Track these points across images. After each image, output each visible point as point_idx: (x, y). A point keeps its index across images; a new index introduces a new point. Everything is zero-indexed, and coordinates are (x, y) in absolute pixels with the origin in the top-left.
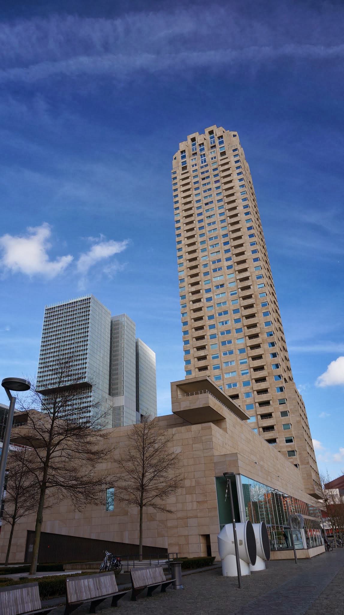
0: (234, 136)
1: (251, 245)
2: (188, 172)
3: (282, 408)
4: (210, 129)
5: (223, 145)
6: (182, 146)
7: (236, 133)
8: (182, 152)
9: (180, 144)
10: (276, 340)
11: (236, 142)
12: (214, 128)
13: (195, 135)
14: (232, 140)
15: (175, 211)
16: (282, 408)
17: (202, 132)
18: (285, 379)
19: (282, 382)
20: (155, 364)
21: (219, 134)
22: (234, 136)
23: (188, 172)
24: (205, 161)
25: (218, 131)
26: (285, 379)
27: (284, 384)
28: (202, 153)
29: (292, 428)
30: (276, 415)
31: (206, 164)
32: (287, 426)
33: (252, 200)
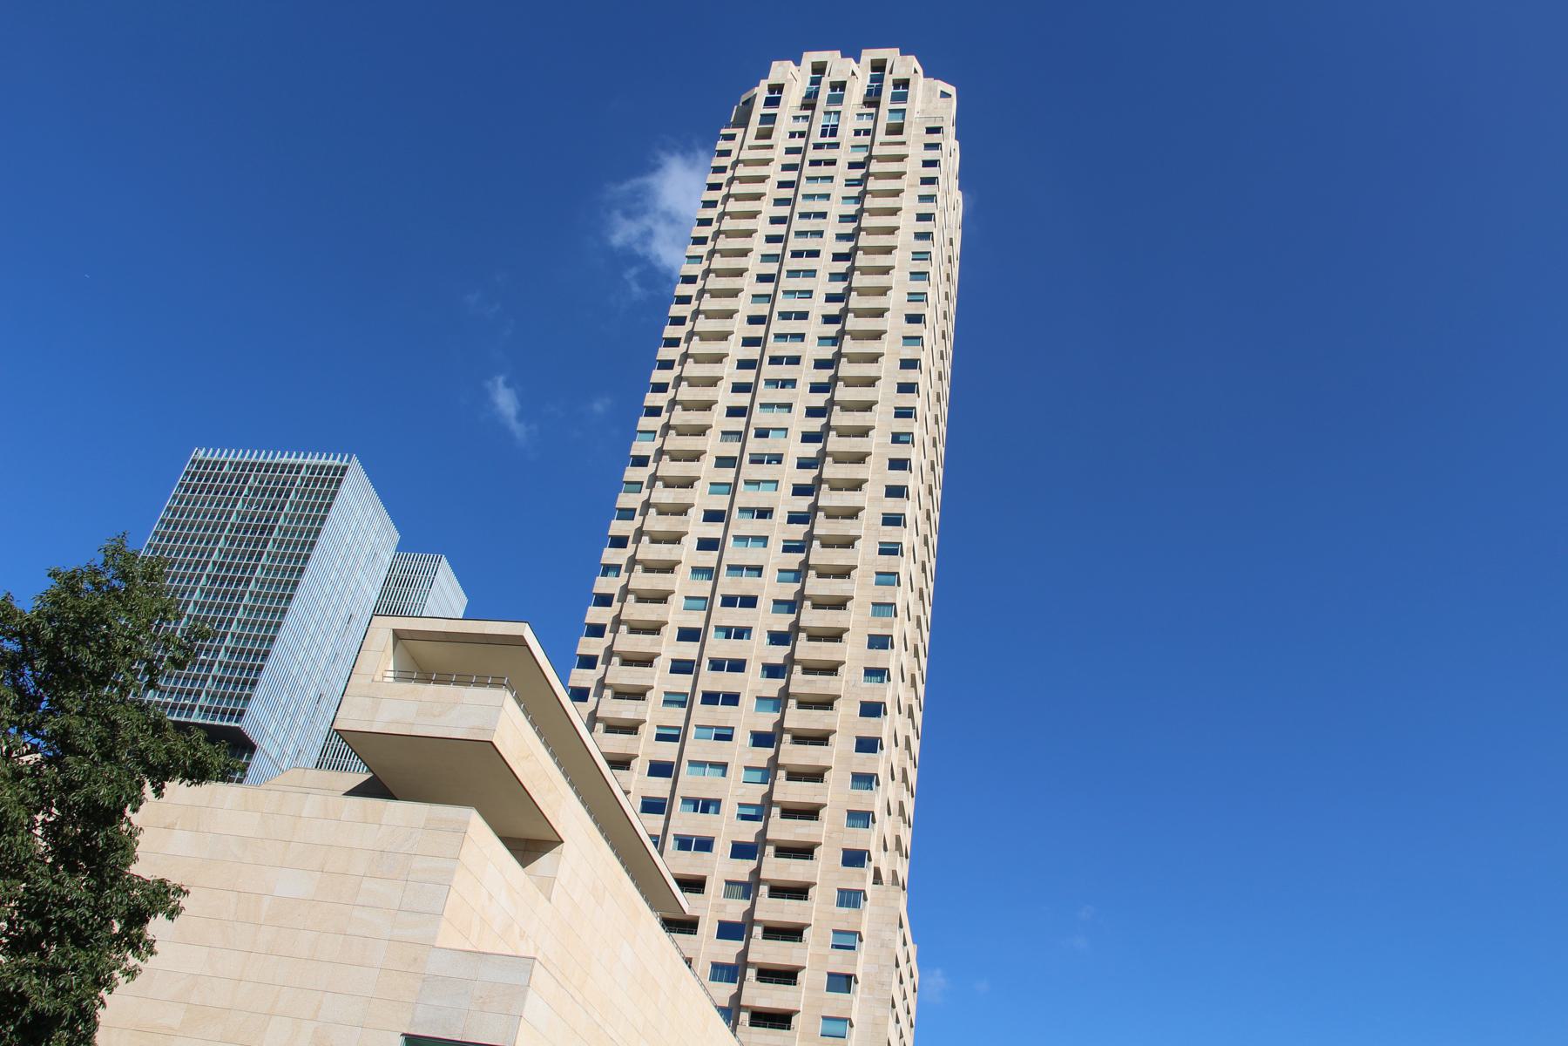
0: (944, 95)
1: (897, 415)
2: (771, 147)
3: (839, 962)
4: (879, 54)
5: (901, 106)
6: (781, 71)
7: (951, 90)
8: (772, 89)
9: (775, 64)
10: (878, 810)
11: (947, 112)
12: (891, 55)
13: (832, 58)
14: (932, 101)
15: (696, 228)
16: (845, 918)
17: (853, 53)
18: (877, 873)
19: (864, 877)
20: (518, 429)
21: (900, 73)
22: (944, 95)
23: (771, 147)
24: (834, 133)
25: (903, 65)
26: (877, 873)
27: (869, 886)
28: (832, 108)
29: (863, 949)
30: (812, 979)
31: (832, 140)
32: (846, 940)
33: (935, 376)
